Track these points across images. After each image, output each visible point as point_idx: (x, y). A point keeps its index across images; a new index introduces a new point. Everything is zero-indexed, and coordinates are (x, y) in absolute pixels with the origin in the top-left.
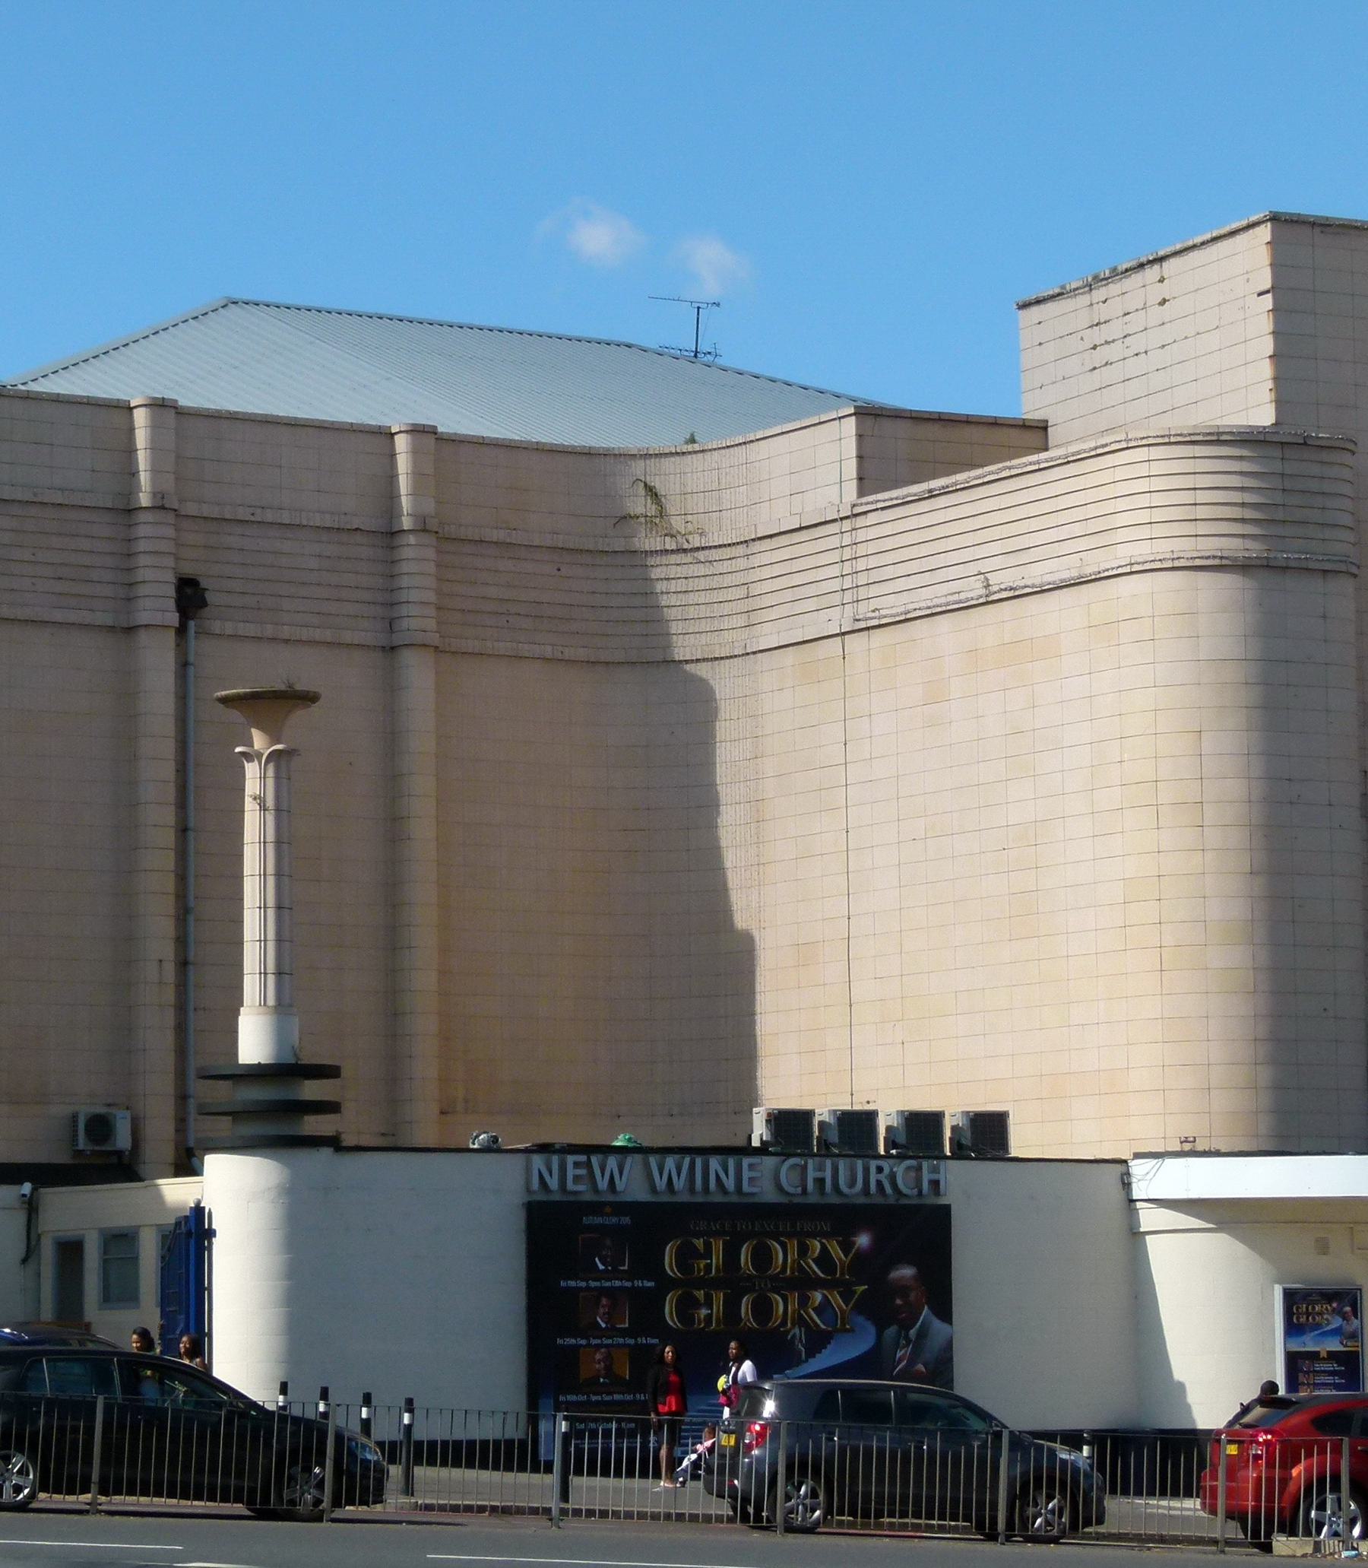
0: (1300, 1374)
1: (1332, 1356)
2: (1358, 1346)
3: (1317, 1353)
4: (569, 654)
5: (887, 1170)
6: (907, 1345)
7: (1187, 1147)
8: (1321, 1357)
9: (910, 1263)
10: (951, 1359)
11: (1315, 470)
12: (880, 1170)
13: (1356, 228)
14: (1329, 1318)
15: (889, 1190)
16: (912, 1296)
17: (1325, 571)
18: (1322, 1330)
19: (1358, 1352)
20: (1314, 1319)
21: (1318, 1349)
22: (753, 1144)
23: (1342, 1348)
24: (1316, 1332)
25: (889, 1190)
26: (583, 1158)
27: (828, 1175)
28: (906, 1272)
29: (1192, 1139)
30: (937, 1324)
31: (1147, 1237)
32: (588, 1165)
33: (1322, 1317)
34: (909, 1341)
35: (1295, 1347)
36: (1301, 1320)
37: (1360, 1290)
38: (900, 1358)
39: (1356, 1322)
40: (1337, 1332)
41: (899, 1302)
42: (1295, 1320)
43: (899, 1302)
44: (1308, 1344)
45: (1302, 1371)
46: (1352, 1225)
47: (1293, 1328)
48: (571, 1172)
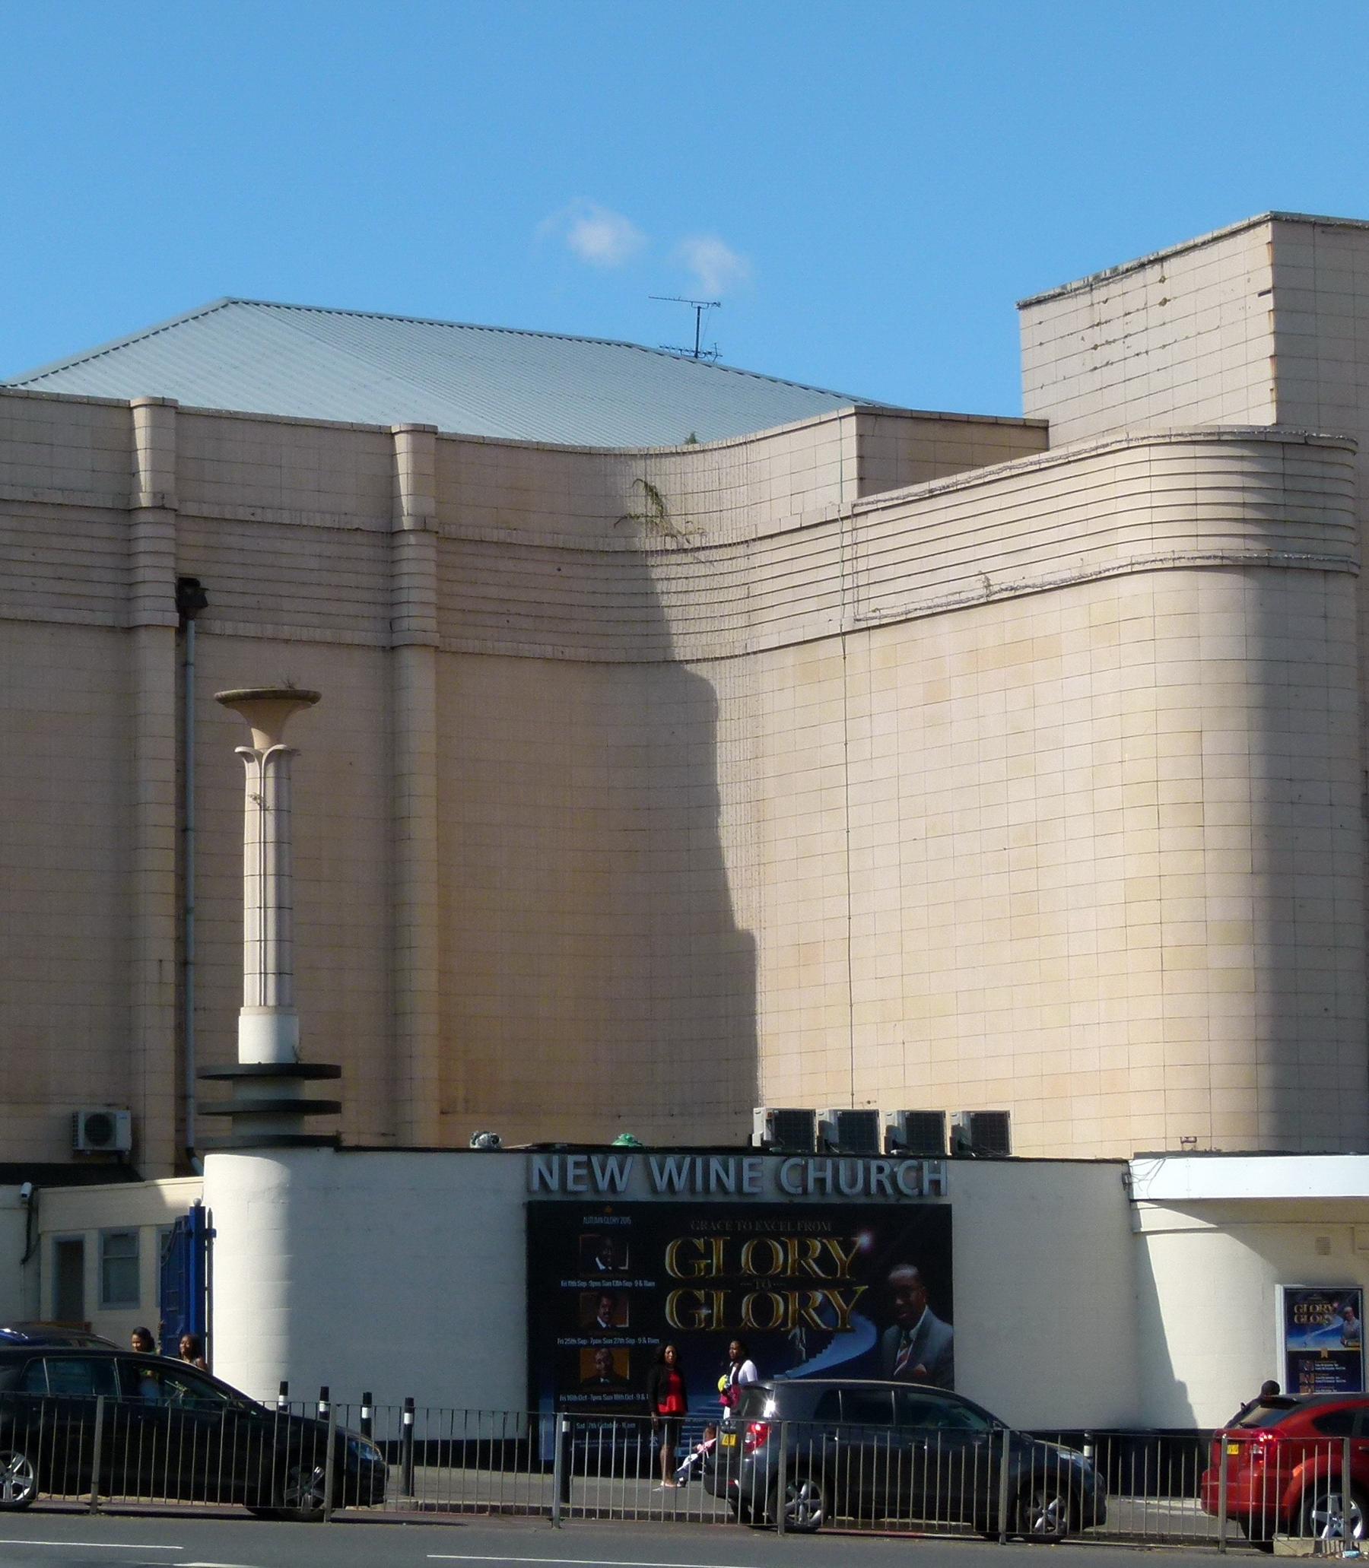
0: (1301, 1374)
1: (1333, 1356)
2: (1359, 1346)
3: (1318, 1353)
4: (569, 653)
5: (887, 1171)
6: (908, 1345)
7: (1188, 1147)
8: (1322, 1356)
9: (910, 1263)
10: (952, 1359)
11: (1316, 470)
12: (880, 1170)
13: (1357, 228)
14: (1331, 1318)
15: (889, 1190)
16: (913, 1296)
17: (1326, 571)
18: (1323, 1330)
19: (1359, 1352)
20: (1315, 1319)
21: (1319, 1349)
22: (754, 1144)
23: (1343, 1349)
24: (1317, 1332)
25: (889, 1190)
26: (583, 1158)
27: (829, 1175)
28: (907, 1272)
29: (1193, 1139)
30: (938, 1324)
31: (1148, 1237)
32: (589, 1165)
33: (1323, 1317)
34: (909, 1341)
35: (1296, 1347)
36: (1302, 1320)
37: (1361, 1290)
38: (900, 1358)
39: (1357, 1322)
40: (1338, 1331)
41: (899, 1302)
42: (1296, 1320)
43: (899, 1302)
44: (1309, 1344)
45: (1303, 1371)
46: (1353, 1225)
47: (1293, 1328)
48: (571, 1172)
